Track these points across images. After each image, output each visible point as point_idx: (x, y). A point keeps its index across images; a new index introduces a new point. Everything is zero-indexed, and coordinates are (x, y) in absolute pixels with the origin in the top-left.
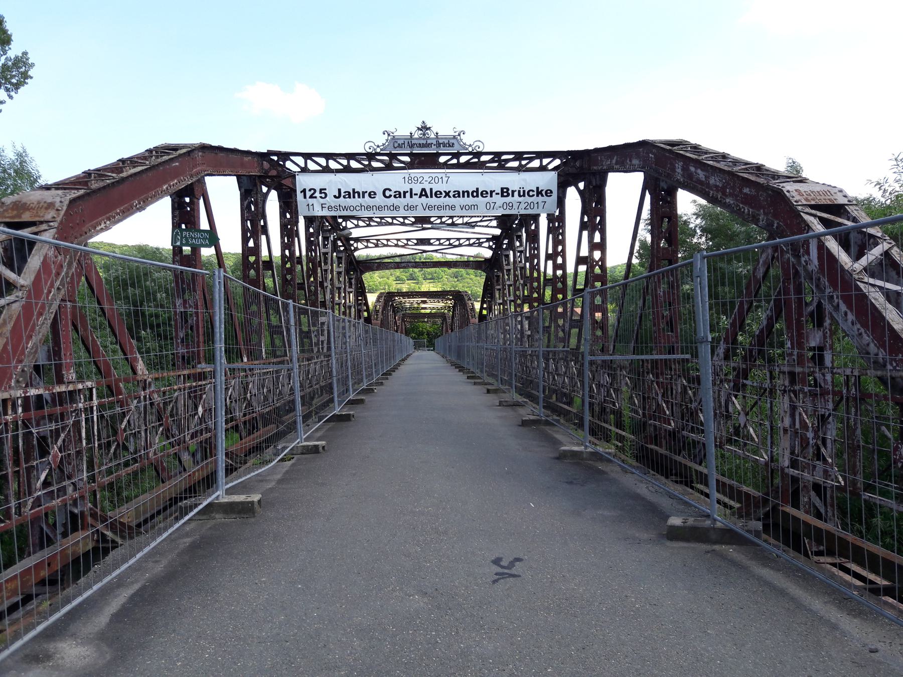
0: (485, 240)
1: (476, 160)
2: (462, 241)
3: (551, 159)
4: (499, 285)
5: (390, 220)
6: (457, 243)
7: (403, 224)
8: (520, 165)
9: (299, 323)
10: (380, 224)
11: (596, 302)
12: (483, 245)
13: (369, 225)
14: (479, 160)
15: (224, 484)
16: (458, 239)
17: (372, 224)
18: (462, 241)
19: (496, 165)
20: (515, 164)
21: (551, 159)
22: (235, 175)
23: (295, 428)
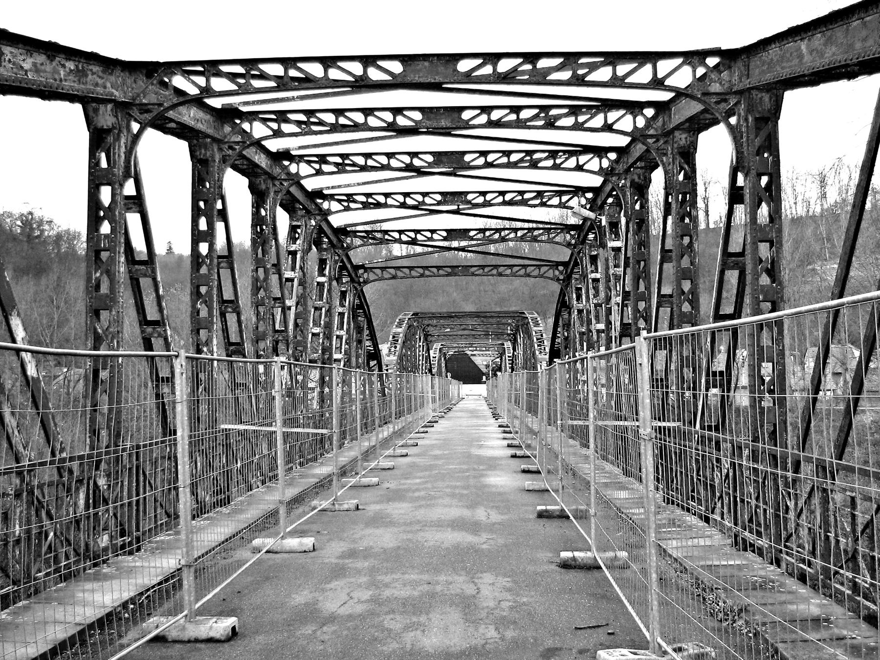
0: (565, 111)
1: (528, 67)
2: (489, 197)
3: (636, 65)
4: (617, 237)
5: (381, 199)
6: (480, 200)
7: (403, 205)
8: (555, 164)
9: (648, 288)
10: (366, 206)
11: (683, 309)
12: (539, 165)
13: (347, 209)
14: (535, 67)
15: (193, 603)
16: (483, 194)
17: (352, 205)
18: (489, 197)
19: (541, 123)
20: (550, 163)
21: (636, 65)
22: (71, 98)
23: (277, 523)
